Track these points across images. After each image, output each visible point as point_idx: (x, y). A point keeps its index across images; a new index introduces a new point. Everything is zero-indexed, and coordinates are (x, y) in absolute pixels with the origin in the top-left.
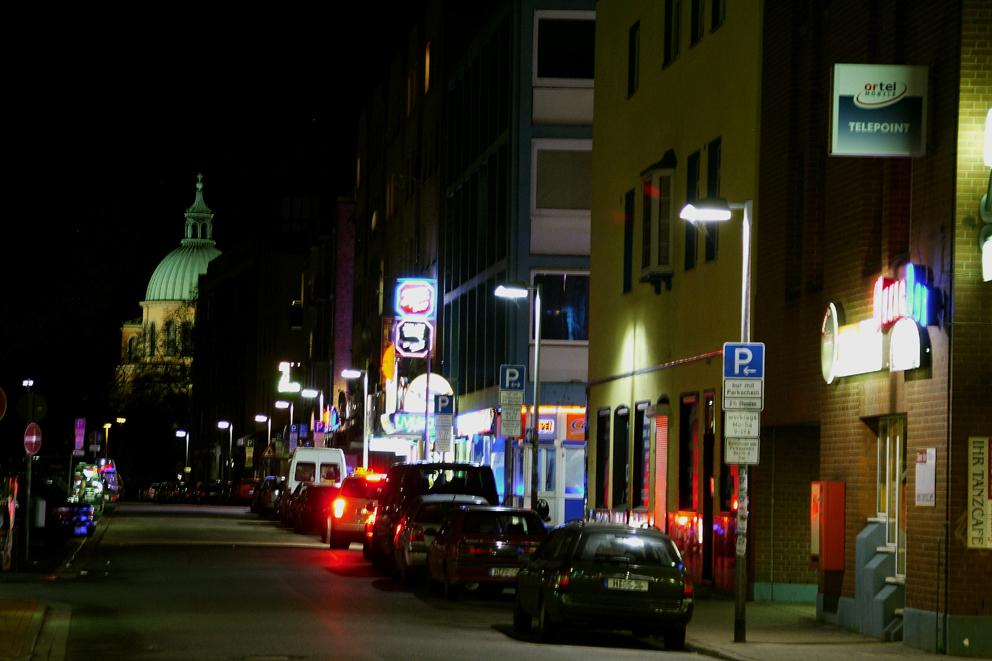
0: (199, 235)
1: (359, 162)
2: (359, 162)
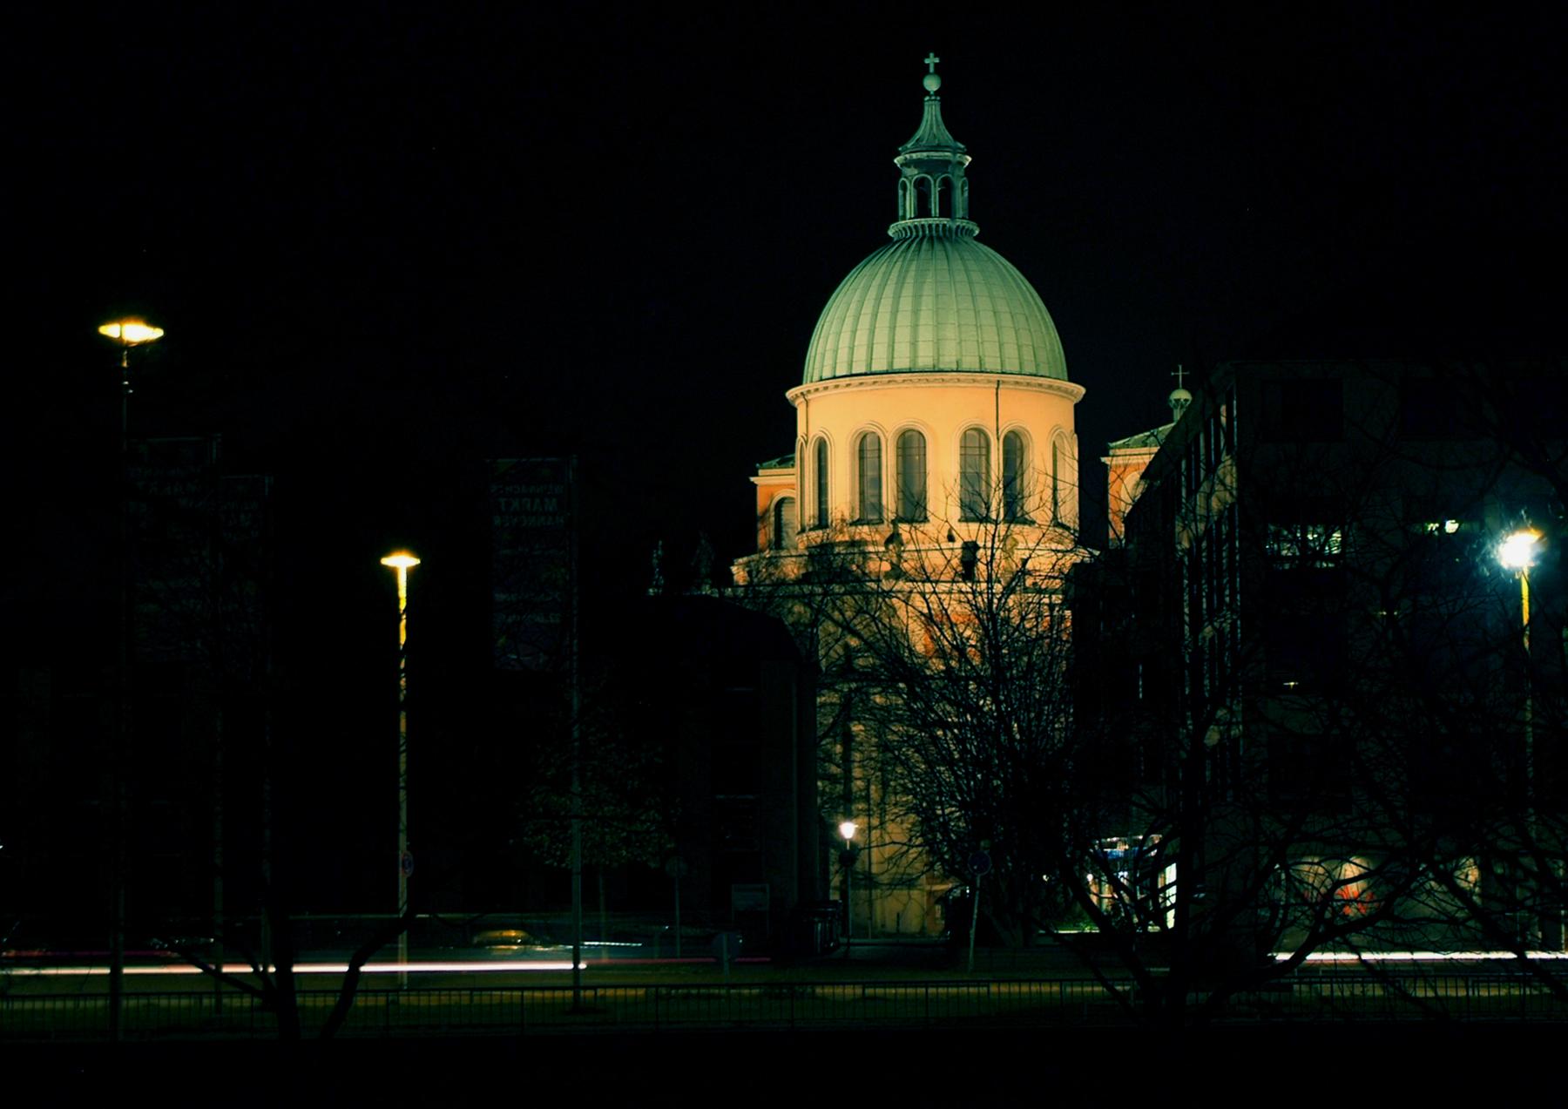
0: (935, 207)
1: (403, 638)
2: (403, 638)
